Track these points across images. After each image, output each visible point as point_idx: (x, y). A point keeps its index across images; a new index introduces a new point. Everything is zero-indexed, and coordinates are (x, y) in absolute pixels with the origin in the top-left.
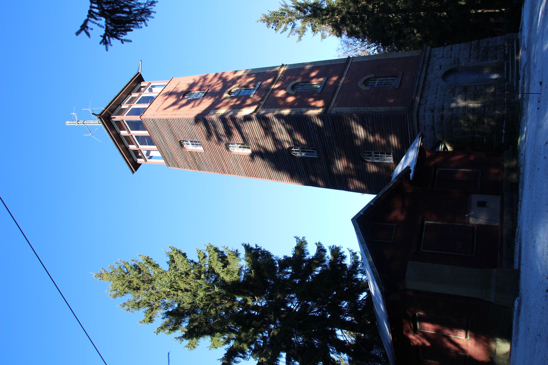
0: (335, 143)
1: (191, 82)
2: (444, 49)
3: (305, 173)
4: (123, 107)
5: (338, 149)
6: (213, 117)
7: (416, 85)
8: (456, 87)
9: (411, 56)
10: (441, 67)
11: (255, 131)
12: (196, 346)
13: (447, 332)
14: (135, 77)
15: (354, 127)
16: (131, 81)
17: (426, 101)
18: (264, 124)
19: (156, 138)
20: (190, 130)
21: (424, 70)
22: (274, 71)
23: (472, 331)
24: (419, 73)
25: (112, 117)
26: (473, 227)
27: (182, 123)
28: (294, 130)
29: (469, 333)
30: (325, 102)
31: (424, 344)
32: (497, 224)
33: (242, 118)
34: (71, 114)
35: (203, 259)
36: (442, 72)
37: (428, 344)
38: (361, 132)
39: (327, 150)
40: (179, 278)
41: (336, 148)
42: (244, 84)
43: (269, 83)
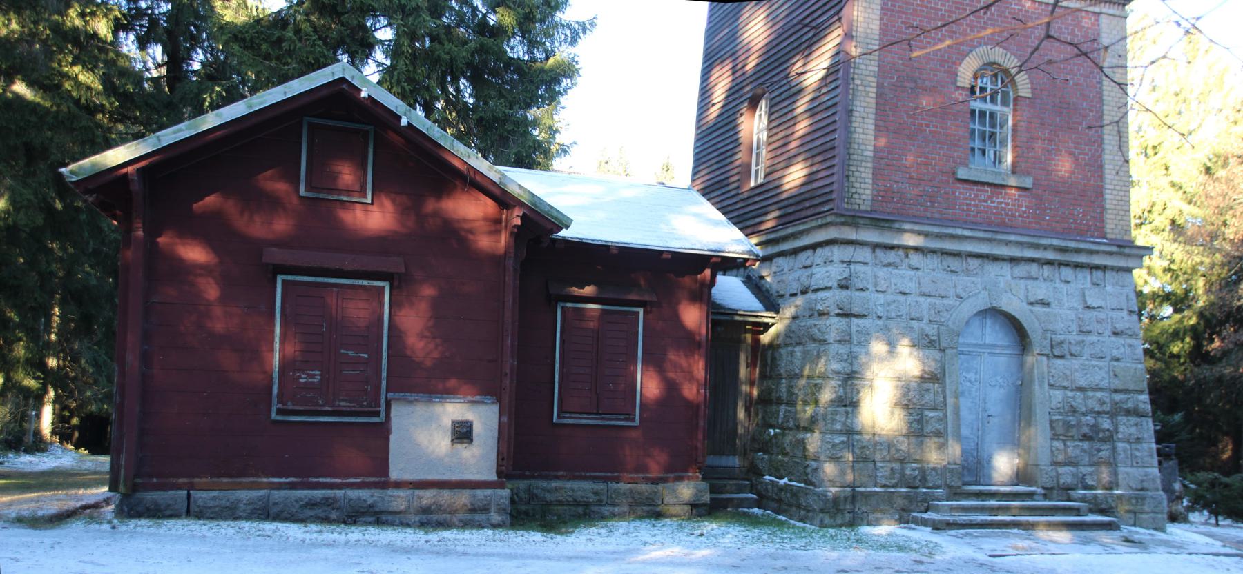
2: (1125, 312)
7: (959, 232)
8: (942, 350)
9: (1103, 209)
24: (1013, 238)
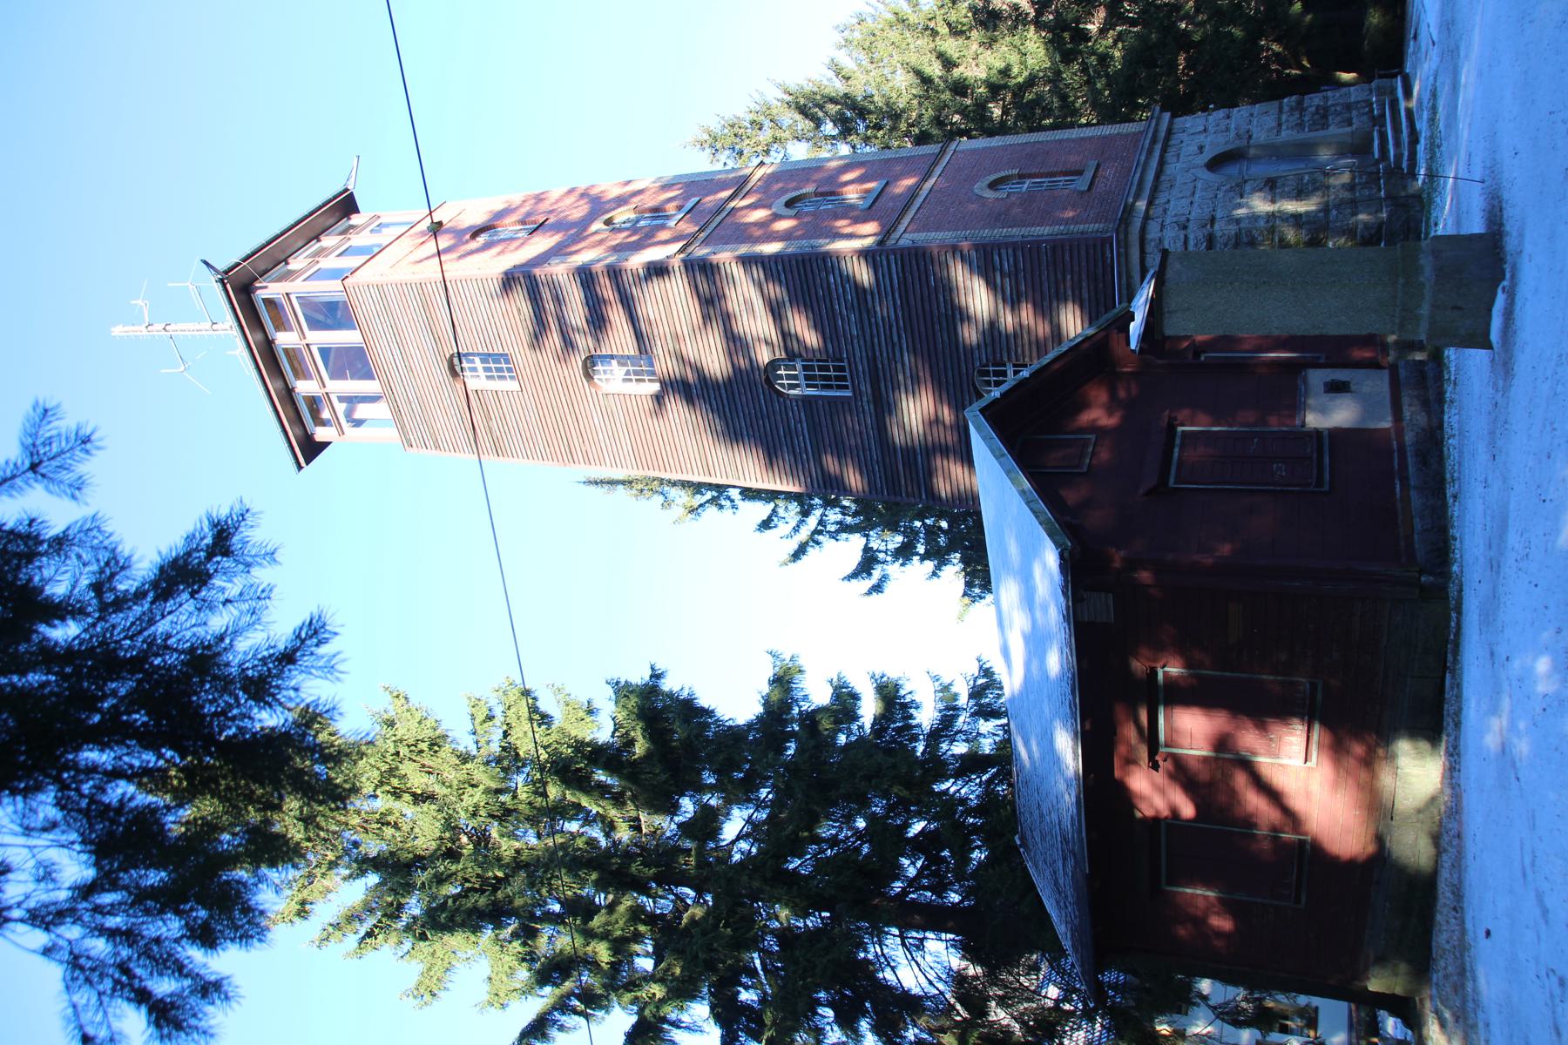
0: (904, 342)
1: (500, 207)
3: (809, 449)
4: (290, 267)
5: (913, 360)
6: (560, 270)
8: (1246, 182)
10: (1201, 148)
11: (675, 313)
12: (442, 994)
13: (1249, 739)
14: (335, 197)
15: (961, 285)
16: (325, 204)
17: (1165, 211)
18: (704, 286)
19: (383, 353)
20: (486, 318)
21: (1157, 153)
22: (735, 177)
23: (1325, 723)
25: (258, 285)
26: (1318, 433)
27: (463, 296)
28: (788, 304)
29: (1317, 727)
30: (882, 225)
31: (1175, 813)
32: (1386, 424)
33: (641, 271)
34: (133, 302)
35: (484, 721)
36: (1207, 156)
37: (1188, 810)
38: (978, 298)
39: (880, 366)
40: (411, 751)
41: (906, 358)
42: (650, 204)
43: (721, 199)
